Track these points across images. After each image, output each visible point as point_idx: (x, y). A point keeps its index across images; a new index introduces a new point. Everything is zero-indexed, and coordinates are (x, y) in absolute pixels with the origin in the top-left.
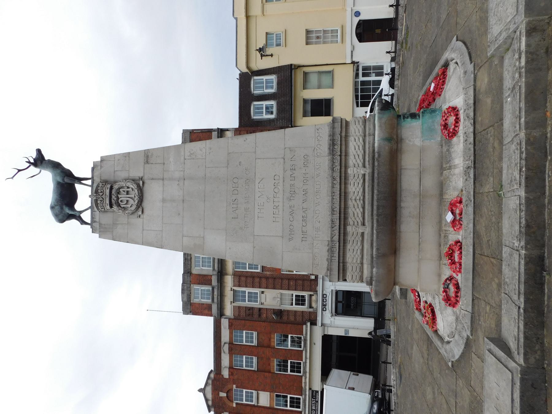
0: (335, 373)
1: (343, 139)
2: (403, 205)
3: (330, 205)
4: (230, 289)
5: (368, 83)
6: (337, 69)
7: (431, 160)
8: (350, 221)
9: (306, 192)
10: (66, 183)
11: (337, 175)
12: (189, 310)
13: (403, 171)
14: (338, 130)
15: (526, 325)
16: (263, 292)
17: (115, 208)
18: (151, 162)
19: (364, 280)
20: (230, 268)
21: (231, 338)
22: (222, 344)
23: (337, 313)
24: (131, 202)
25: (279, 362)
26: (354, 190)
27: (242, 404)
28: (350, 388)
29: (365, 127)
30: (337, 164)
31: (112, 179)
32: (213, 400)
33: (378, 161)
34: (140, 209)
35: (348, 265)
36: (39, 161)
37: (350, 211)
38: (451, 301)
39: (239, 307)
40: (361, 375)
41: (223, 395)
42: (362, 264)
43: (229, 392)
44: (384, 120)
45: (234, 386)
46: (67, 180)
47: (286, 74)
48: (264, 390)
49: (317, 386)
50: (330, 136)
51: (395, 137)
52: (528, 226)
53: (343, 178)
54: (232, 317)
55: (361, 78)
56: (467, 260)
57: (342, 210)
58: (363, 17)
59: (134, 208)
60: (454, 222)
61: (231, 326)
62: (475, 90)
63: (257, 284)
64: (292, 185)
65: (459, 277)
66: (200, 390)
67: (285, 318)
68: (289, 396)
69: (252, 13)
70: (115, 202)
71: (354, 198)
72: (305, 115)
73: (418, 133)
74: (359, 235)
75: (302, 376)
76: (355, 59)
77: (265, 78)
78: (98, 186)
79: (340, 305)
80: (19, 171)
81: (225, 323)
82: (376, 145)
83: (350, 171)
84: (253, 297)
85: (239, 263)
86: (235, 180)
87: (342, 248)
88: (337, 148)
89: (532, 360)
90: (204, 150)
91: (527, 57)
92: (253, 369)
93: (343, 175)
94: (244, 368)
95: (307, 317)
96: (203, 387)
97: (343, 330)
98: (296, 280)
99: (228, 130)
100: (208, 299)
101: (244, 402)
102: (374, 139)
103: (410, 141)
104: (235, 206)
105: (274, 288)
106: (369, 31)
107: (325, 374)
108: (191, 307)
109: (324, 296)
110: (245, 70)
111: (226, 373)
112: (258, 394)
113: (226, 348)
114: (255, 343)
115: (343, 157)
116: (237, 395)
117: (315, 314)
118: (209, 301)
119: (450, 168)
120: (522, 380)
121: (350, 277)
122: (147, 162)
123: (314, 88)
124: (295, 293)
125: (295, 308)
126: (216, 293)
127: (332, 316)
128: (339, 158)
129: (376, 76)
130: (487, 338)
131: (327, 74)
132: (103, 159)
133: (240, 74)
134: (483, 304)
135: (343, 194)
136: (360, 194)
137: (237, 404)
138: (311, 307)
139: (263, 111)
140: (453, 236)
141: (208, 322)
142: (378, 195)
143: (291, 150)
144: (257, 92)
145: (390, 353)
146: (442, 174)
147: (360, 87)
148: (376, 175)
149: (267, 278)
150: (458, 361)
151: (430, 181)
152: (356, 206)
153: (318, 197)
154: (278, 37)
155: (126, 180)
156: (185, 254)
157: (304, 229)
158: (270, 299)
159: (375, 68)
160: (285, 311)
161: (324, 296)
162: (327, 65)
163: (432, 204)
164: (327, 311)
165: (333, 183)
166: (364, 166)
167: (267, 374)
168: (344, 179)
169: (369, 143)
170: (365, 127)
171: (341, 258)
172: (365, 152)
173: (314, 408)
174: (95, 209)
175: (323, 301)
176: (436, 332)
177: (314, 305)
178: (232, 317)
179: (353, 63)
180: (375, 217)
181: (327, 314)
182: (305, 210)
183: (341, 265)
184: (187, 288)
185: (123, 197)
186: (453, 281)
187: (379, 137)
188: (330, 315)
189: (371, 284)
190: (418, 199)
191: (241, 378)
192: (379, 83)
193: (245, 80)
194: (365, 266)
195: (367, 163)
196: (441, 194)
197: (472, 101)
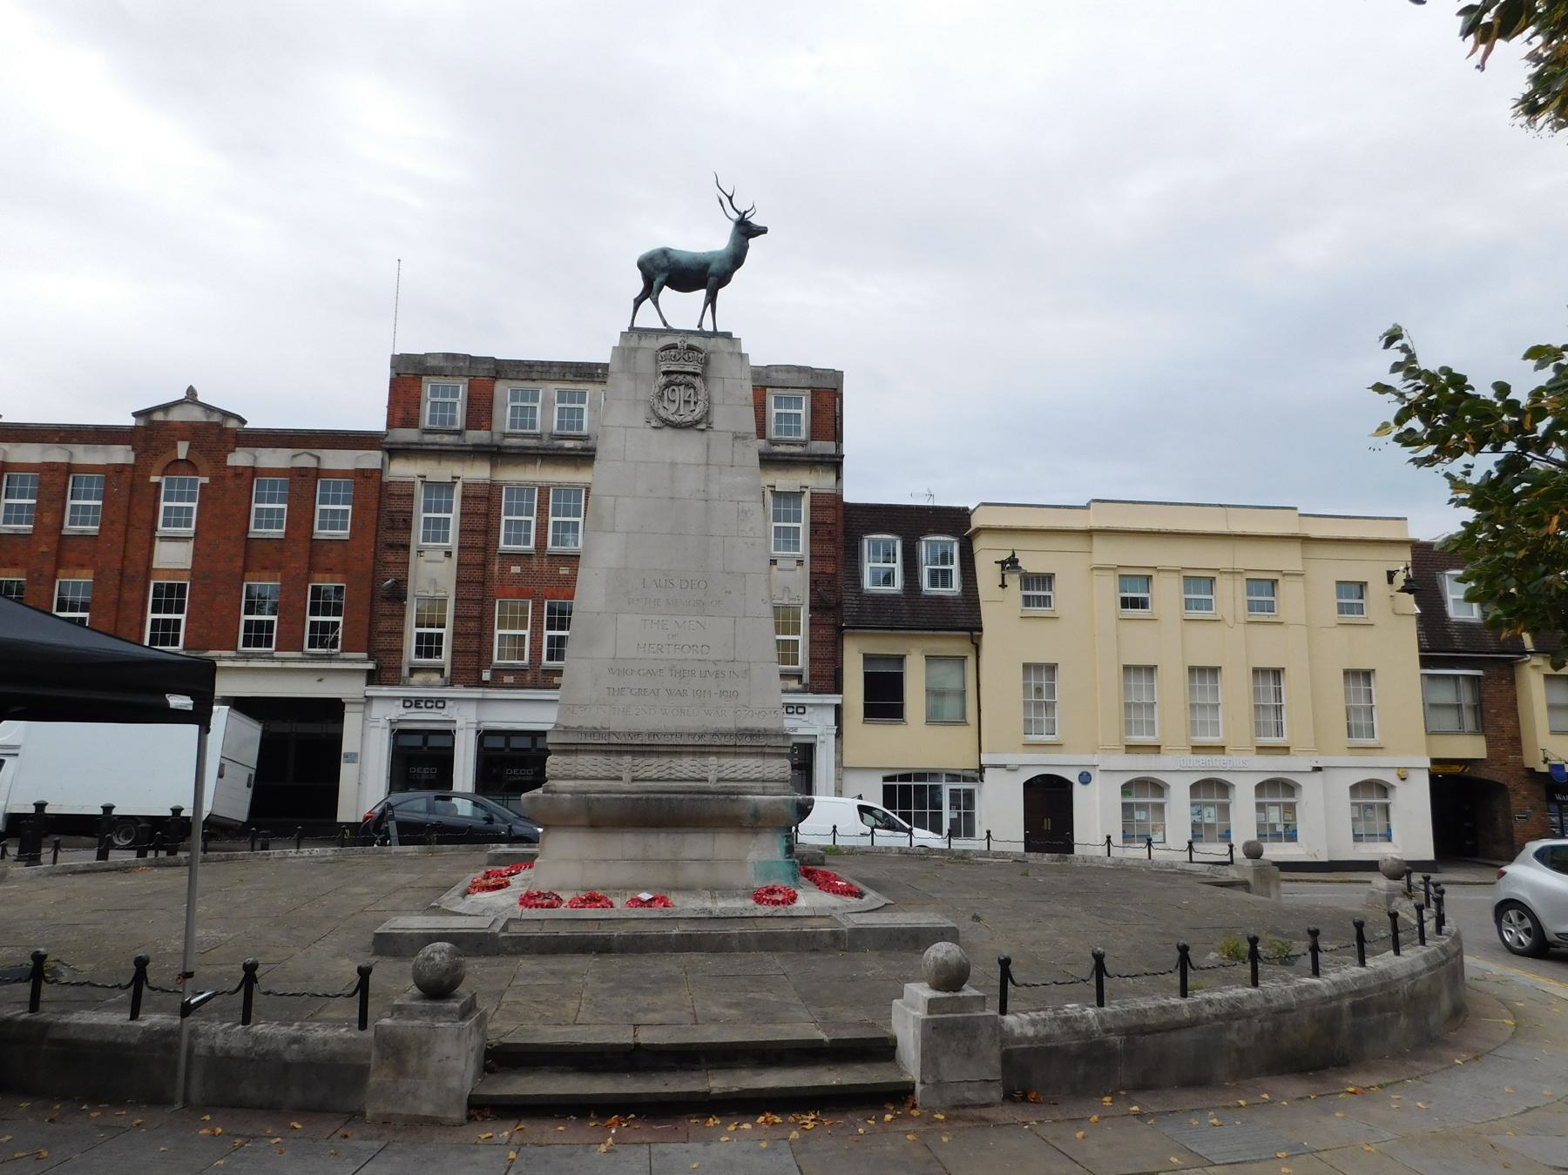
0: (252, 731)
2: (662, 835)
6: (968, 733)
7: (726, 874)
8: (638, 761)
9: (682, 694)
11: (707, 740)
12: (402, 370)
14: (773, 742)
16: (448, 554)
17: (663, 380)
21: (332, 473)
22: (316, 452)
23: (398, 734)
24: (673, 408)
27: (157, 499)
28: (222, 766)
30: (724, 741)
31: (711, 373)
34: (659, 424)
36: (746, 230)
37: (653, 761)
39: (411, 496)
40: (247, 794)
41: (182, 450)
42: (576, 778)
43: (190, 465)
44: (783, 807)
45: (206, 480)
47: (960, 619)
52: (642, 937)
54: (386, 479)
55: (947, 788)
58: (1079, 792)
59: (663, 413)
61: (362, 474)
63: (469, 542)
64: (693, 673)
66: (191, 392)
67: (385, 608)
68: (182, 617)
69: (1098, 544)
70: (673, 379)
72: (868, 659)
73: (766, 856)
79: (417, 741)
80: (730, 198)
81: (370, 459)
83: (712, 760)
84: (437, 529)
86: (702, 585)
88: (747, 741)
89: (505, 944)
94: (255, 506)
96: (200, 398)
99: (839, 478)
101: (163, 504)
105: (459, 583)
106: (1049, 803)
108: (409, 377)
109: (440, 702)
110: (977, 521)
111: (239, 458)
112: (186, 539)
113: (305, 460)
114: (320, 533)
116: (182, 484)
117: (396, 681)
118: (426, 422)
119: (713, 898)
122: (736, 438)
123: (927, 678)
124: (447, 632)
125: (411, 632)
126: (447, 439)
129: (952, 820)
131: (951, 708)
133: (966, 509)
137: (158, 485)
138: (414, 670)
139: (878, 568)
140: (619, 902)
141: (372, 416)
143: (747, 672)
149: (484, 566)
151: (695, 873)
154: (1045, 601)
155: (709, 400)
158: (433, 572)
159: (970, 817)
160: (403, 608)
161: (440, 702)
163: (663, 876)
164: (404, 711)
166: (719, 780)
168: (701, 751)
177: (418, 678)
178: (386, 479)
179: (981, 769)
181: (396, 711)
182: (655, 693)
184: (460, 369)
185: (681, 393)
188: (393, 717)
191: (226, 501)
192: (937, 829)
193: (954, 521)
194: (571, 783)
196: (678, 889)
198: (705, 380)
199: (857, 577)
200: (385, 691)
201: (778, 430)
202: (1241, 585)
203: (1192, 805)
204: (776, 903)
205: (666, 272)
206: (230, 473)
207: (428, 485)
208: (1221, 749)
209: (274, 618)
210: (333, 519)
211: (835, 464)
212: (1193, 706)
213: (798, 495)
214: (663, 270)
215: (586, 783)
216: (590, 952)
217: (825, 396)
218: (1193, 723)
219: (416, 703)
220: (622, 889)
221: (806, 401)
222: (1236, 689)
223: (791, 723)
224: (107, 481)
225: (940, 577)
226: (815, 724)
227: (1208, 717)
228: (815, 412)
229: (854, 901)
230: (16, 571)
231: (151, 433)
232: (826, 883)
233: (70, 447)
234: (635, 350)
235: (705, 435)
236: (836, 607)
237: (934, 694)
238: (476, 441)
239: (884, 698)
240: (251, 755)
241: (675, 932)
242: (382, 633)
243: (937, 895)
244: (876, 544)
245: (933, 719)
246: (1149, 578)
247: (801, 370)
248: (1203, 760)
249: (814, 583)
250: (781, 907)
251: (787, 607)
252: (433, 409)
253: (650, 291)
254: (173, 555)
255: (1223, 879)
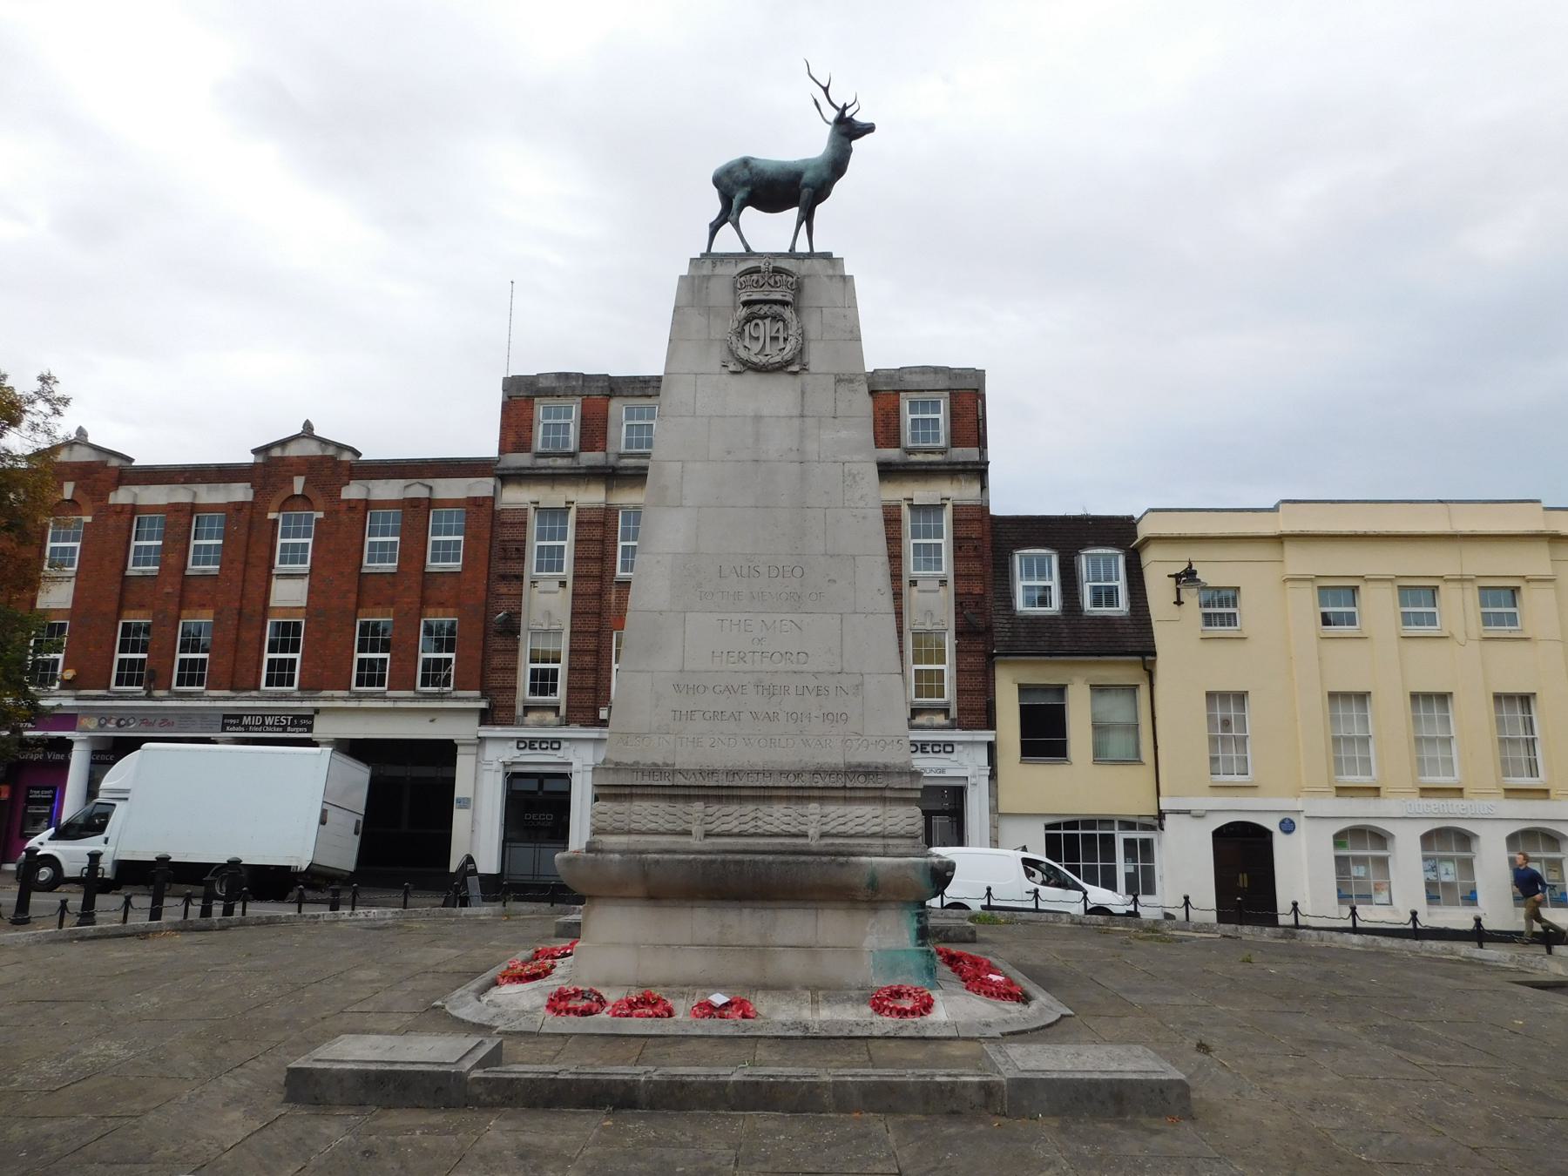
1: (878, 793)
2: (746, 912)
3: (747, 767)
4: (571, 499)
5: (1109, 854)
6: (1144, 774)
7: (833, 967)
10: (799, 192)
11: (806, 781)
13: (812, 912)
14: (896, 782)
15: (531, 1081)
17: (743, 312)
18: (840, 390)
19: (598, 837)
20: (626, 498)
22: (429, 482)
23: (513, 778)
24: (756, 347)
25: (385, 630)
26: (776, 815)
28: (324, 812)
29: (902, 837)
30: (828, 782)
31: (807, 300)
32: (282, 459)
33: (830, 863)
34: (739, 368)
35: (627, 805)
36: (848, 129)
37: (733, 808)
38: (558, 1003)
39: (524, 524)
40: (356, 841)
41: (298, 485)
42: (629, 832)
43: (305, 500)
44: (911, 873)
45: (320, 515)
46: (806, 193)
47: (1130, 641)
48: (311, 591)
49: (324, 728)
50: (886, 766)
51: (880, 896)
53: (800, 793)
54: (498, 507)
55: (1120, 837)
56: (636, 1025)
57: (735, 792)
58: (1280, 842)
59: (743, 354)
60: (709, 1005)
61: (475, 503)
62: (950, 1039)
64: (786, 689)
65: (604, 1015)
66: (308, 426)
67: (499, 643)
69: (1290, 550)
70: (754, 311)
71: (760, 815)
72: (1024, 689)
73: (890, 943)
74: (686, 826)
75: (348, 688)
76: (1169, 821)
77: (1121, 584)
78: (788, 273)
79: (532, 785)
80: (826, 90)
81: (482, 487)
82: (864, 859)
83: (813, 807)
84: (550, 559)
85: (637, 522)
86: (798, 572)
87: (661, 791)
88: (860, 782)
89: (478, 1090)
90: (862, 504)
91: (946, 1083)
92: (365, 563)
93: (806, 793)
95: (502, 699)
96: (316, 433)
97: (470, 795)
98: (596, 670)
99: (984, 487)
100: (545, 443)
101: (280, 541)
102: (876, 855)
103: (873, 926)
104: (745, 571)
105: (574, 614)
106: (1244, 856)
107: (354, 749)
108: (521, 399)
109: (555, 744)
110: (1143, 531)
111: (353, 491)
113: (417, 490)
114: (433, 566)
115: (841, 793)
116: (298, 520)
117: (510, 721)
118: (538, 446)
119: (814, 1002)
120: (448, 1074)
121: (601, 809)
122: (839, 380)
124: (562, 668)
125: (525, 668)
126: (560, 462)
127: (505, 765)
128: (839, 784)
129: (1127, 874)
130: (499, 1046)
131: (1125, 745)
132: (847, 281)
133: (1132, 518)
134: (559, 1047)
135: (767, 793)
136: (768, 827)
137: (276, 522)
140: (682, 1008)
141: (484, 442)
142: (763, 862)
144: (1083, 563)
145: (426, 911)
146: (807, 988)
147: (1098, 832)
148: (803, 858)
149: (600, 595)
150: (447, 1015)
151: (790, 965)
152: (743, 819)
153: (763, 742)
154: (1230, 619)
155: (803, 334)
156: (659, 379)
157: (698, 716)
158: (547, 605)
159: (1149, 873)
161: (555, 744)
162: (1156, 748)
163: (747, 969)
164: (517, 753)
165: (789, 772)
167: (353, 597)
168: (798, 795)
169: (868, 845)
170: (902, 837)
171: (639, 791)
172: (851, 836)
173: (268, 721)
174: (743, 266)
175: (544, 740)
176: (495, 983)
177: (533, 717)
178: (498, 507)
179: (1161, 815)
180: (719, 857)
181: (510, 753)
182: (736, 716)
183: (627, 791)
185: (766, 328)
186: (596, 1006)
187: (879, 864)
189: (589, 850)
190: (757, 942)
191: (341, 533)
192: (1110, 884)
193: (1117, 532)
194: (624, 839)
195: (829, 841)
197: (928, 1034)
198: (797, 311)
199: (1008, 598)
200: (498, 731)
201: (915, 437)
202: (1472, 595)
203: (1425, 859)
204: (903, 1013)
205: (754, 187)
206: (344, 507)
207: (913, 508)
208: (1458, 792)
209: (387, 656)
210: (444, 551)
211: (979, 472)
212: (1418, 740)
213: (939, 508)
214: (744, 184)
215: (643, 838)
216: (602, 1106)
217: (966, 398)
218: (1420, 761)
219: (530, 744)
220: (688, 985)
221: (944, 405)
222: (1473, 720)
223: (928, 764)
224: (227, 522)
225: (1109, 596)
226: (963, 763)
227: (1439, 753)
228: (954, 416)
229: (1014, 1008)
230: (142, 613)
231: (269, 469)
232: (974, 976)
233: (194, 487)
234: (708, 278)
235: (798, 380)
236: (986, 631)
237: (1099, 728)
238: (592, 463)
239: (1044, 734)
240: (359, 799)
241: (733, 1078)
242: (495, 670)
243: (1134, 998)
244: (1028, 560)
245: (1100, 757)
246: (1355, 589)
247: (937, 370)
248: (1435, 805)
249: (959, 605)
250: (908, 1020)
251: (928, 633)
252: (546, 432)
253: (728, 214)
254: (289, 593)
255: (1540, 977)
